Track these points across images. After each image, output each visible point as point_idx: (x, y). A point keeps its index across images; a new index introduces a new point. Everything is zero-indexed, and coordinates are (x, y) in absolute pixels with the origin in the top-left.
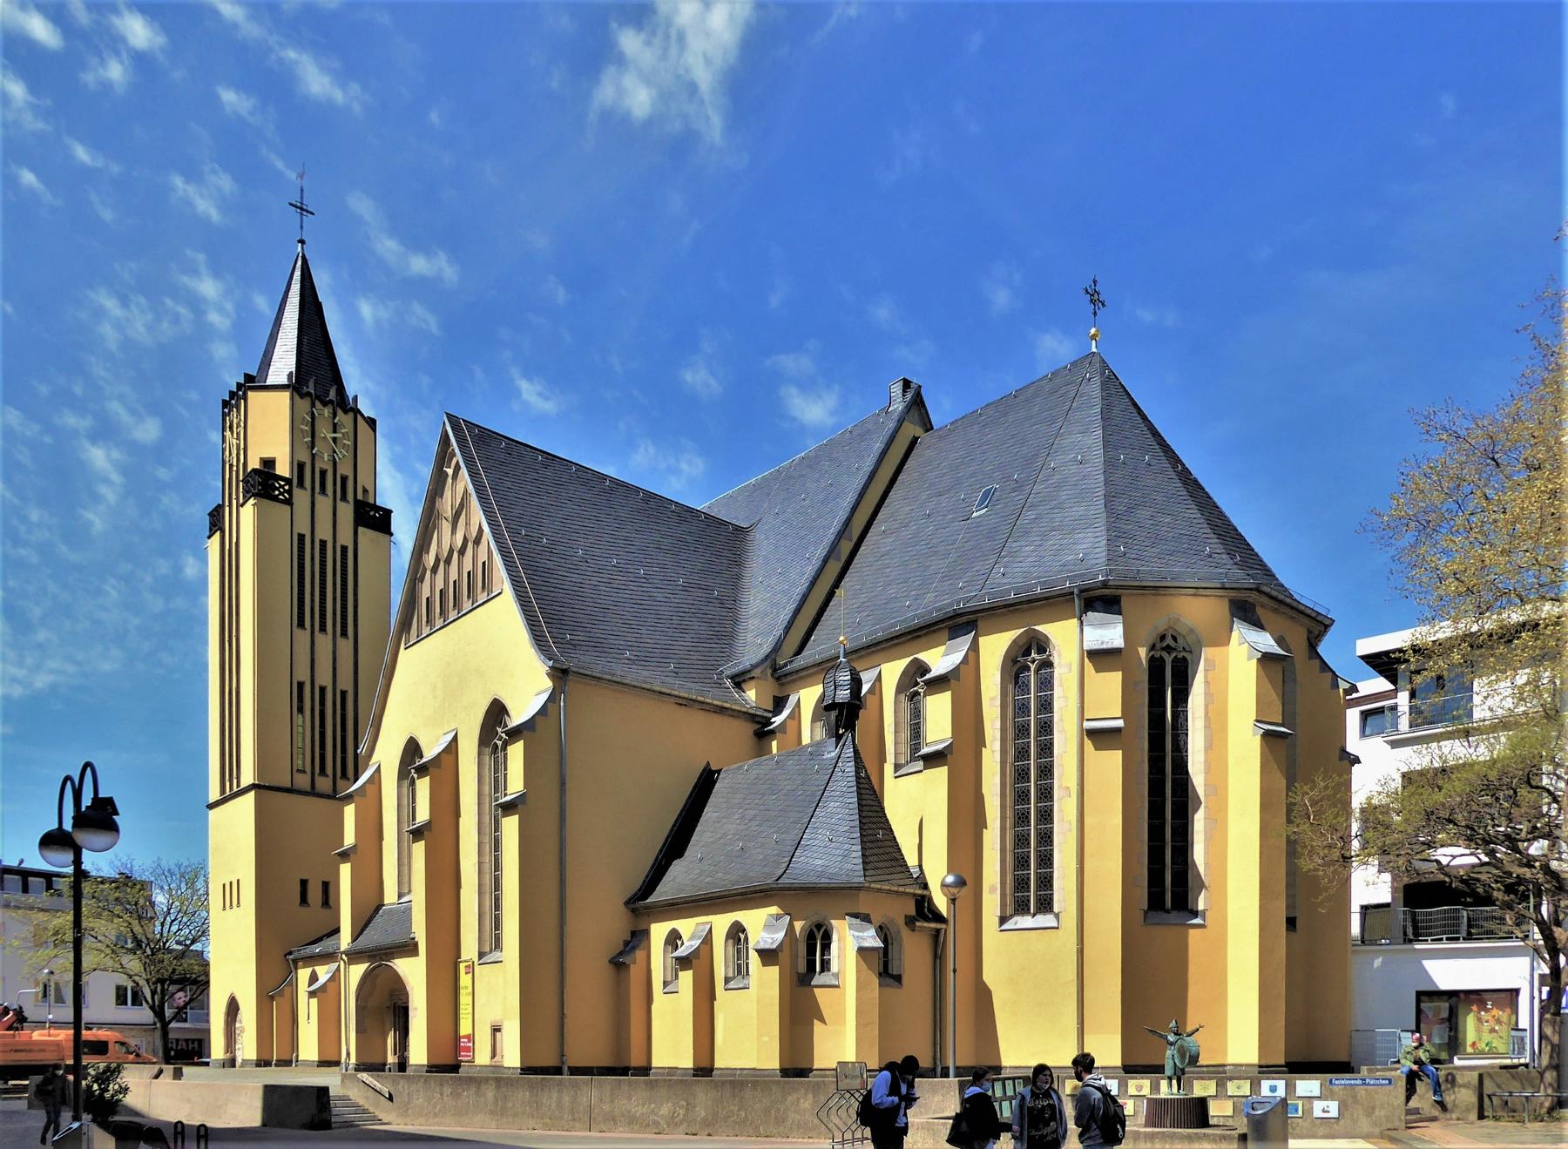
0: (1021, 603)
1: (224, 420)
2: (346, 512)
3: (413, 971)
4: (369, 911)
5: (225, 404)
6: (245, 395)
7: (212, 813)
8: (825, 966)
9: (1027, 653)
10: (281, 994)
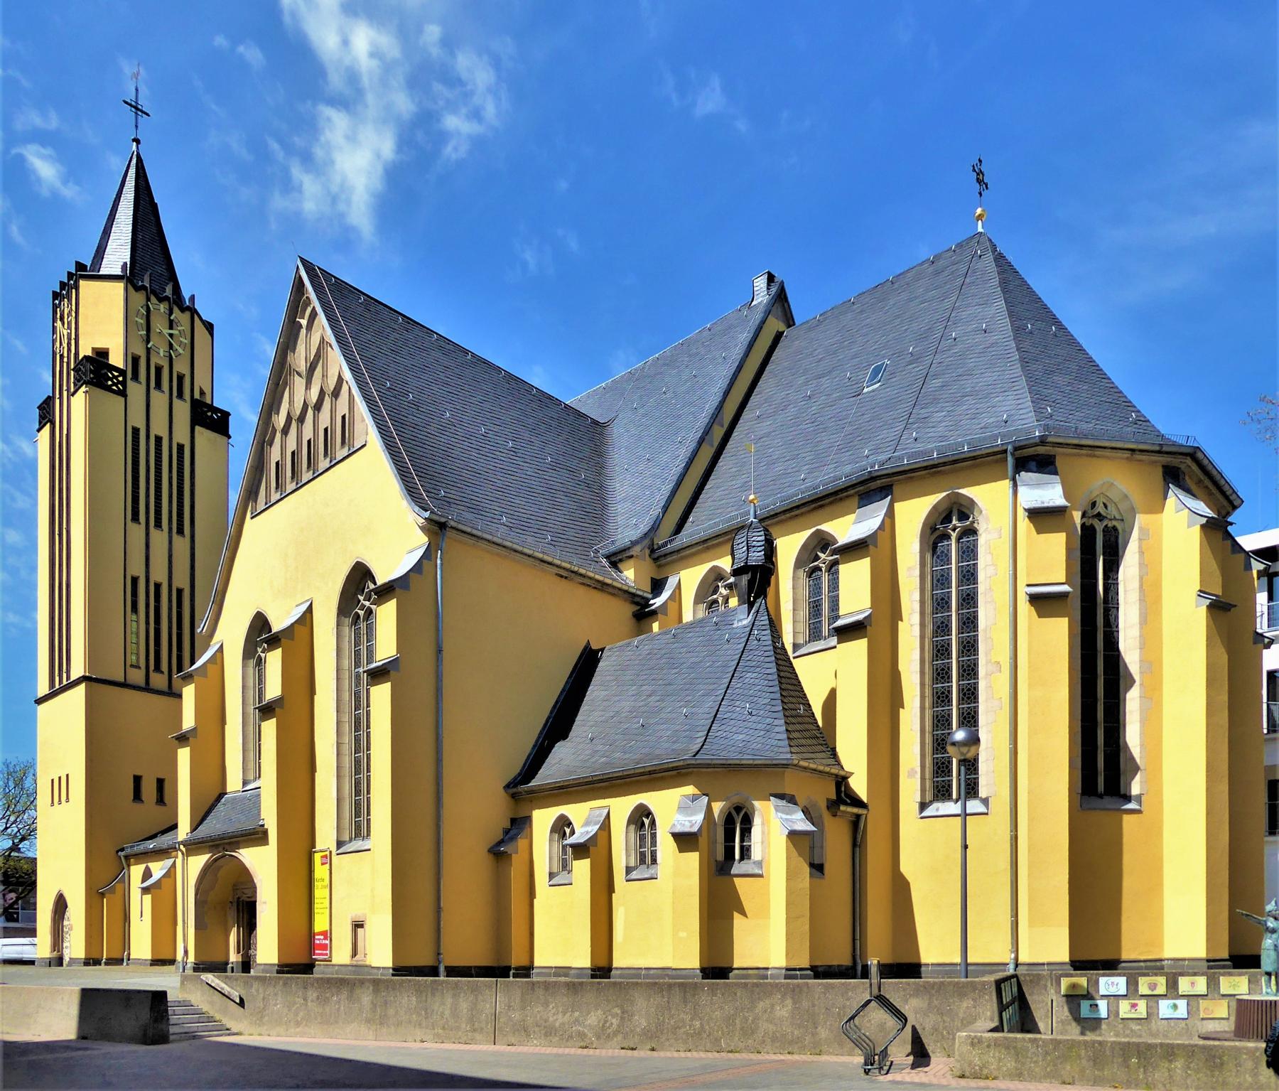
0: (945, 464)
1: (55, 313)
2: (183, 410)
3: (261, 863)
4: (210, 799)
5: (56, 295)
6: (77, 287)
7: (42, 708)
8: (746, 852)
9: (948, 519)
10: (112, 891)
